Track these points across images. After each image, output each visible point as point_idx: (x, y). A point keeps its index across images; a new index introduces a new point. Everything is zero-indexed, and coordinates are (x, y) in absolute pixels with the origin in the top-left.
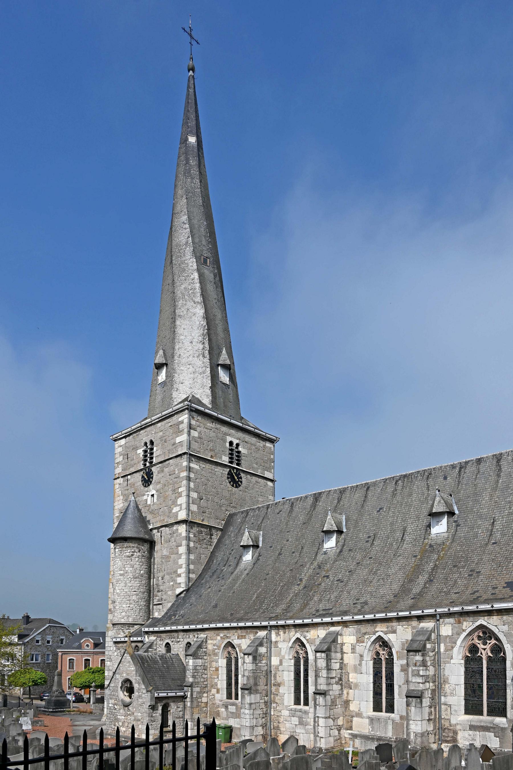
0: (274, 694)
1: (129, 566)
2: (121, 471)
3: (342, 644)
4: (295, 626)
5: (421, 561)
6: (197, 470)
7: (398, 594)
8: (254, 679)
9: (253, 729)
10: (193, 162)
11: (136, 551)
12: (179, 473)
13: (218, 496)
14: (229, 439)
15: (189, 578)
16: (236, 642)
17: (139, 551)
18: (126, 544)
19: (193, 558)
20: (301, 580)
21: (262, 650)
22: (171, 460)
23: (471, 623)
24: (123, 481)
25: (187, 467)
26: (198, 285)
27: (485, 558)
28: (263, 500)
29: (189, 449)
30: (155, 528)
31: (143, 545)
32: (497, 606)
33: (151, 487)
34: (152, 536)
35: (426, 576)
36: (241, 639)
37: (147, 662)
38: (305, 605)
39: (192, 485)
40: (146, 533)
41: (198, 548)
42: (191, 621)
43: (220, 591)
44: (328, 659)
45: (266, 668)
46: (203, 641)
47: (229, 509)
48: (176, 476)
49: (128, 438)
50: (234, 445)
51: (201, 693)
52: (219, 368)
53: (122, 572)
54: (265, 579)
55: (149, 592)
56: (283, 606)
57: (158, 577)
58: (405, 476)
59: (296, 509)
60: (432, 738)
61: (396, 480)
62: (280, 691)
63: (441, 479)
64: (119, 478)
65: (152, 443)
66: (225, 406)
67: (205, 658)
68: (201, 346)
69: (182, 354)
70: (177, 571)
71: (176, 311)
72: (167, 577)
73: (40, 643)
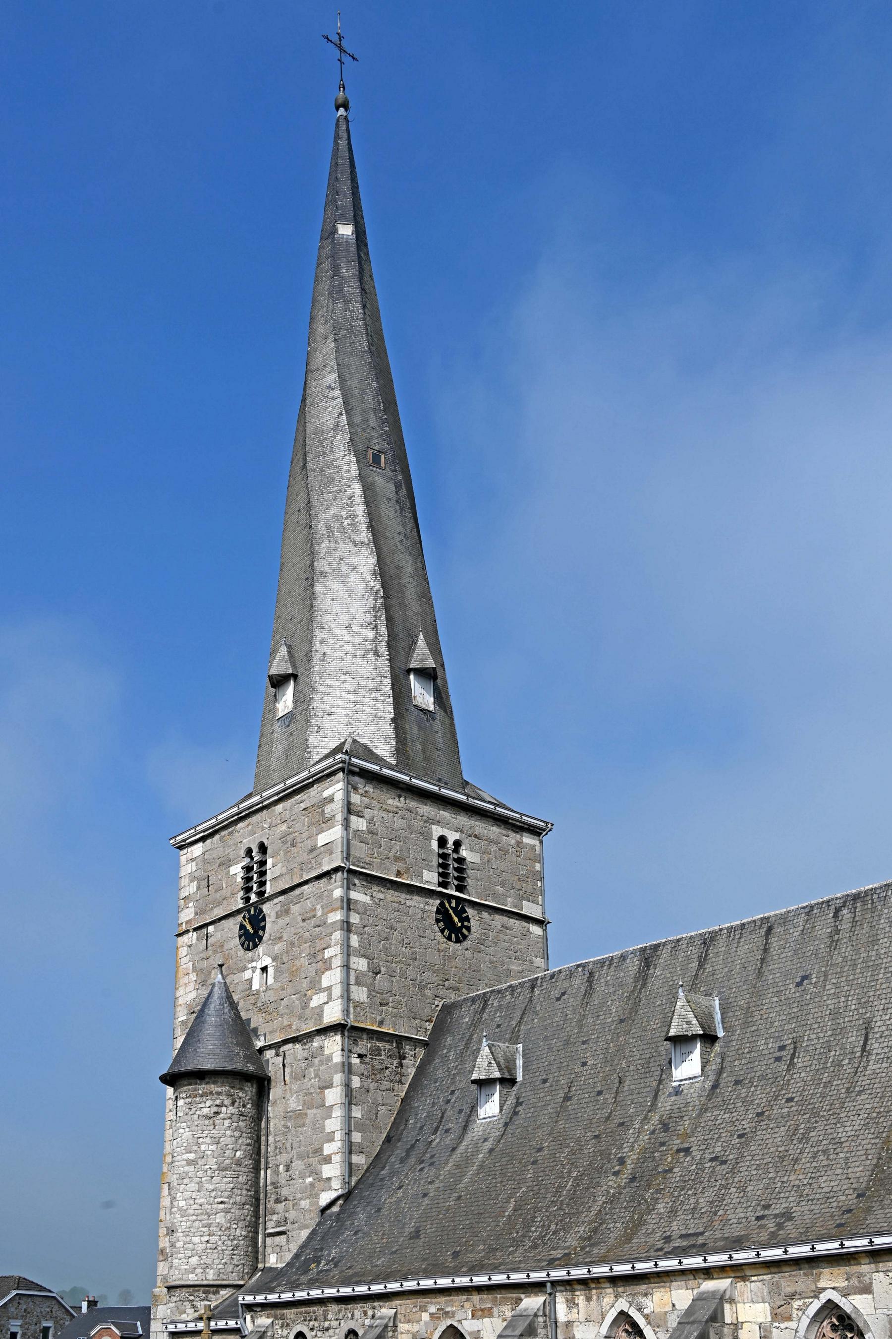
1: (208, 1140)
2: (192, 916)
4: (614, 1280)
7: (868, 1188)
10: (348, 271)
11: (226, 1102)
12: (325, 914)
13: (416, 963)
14: (437, 831)
15: (350, 1164)
17: (233, 1104)
18: (202, 1088)
19: (360, 1116)
20: (622, 1161)
22: (306, 887)
24: (198, 939)
25: (342, 901)
26: (361, 509)
28: (520, 969)
29: (348, 859)
30: (270, 1047)
31: (241, 1089)
33: (261, 949)
34: (262, 1065)
36: (482, 1317)
38: (638, 1225)
39: (355, 940)
40: (248, 1058)
41: (372, 1091)
42: (356, 1274)
43: (425, 1195)
46: (386, 1326)
47: (441, 993)
48: (318, 923)
49: (208, 841)
50: (450, 844)
52: (412, 677)
53: (192, 1156)
54: (535, 1162)
55: (256, 1203)
57: (277, 1166)
58: (856, 897)
59: (600, 988)
64: (187, 932)
65: (263, 848)
66: (427, 759)
68: (371, 634)
71: (316, 564)
72: (298, 1165)
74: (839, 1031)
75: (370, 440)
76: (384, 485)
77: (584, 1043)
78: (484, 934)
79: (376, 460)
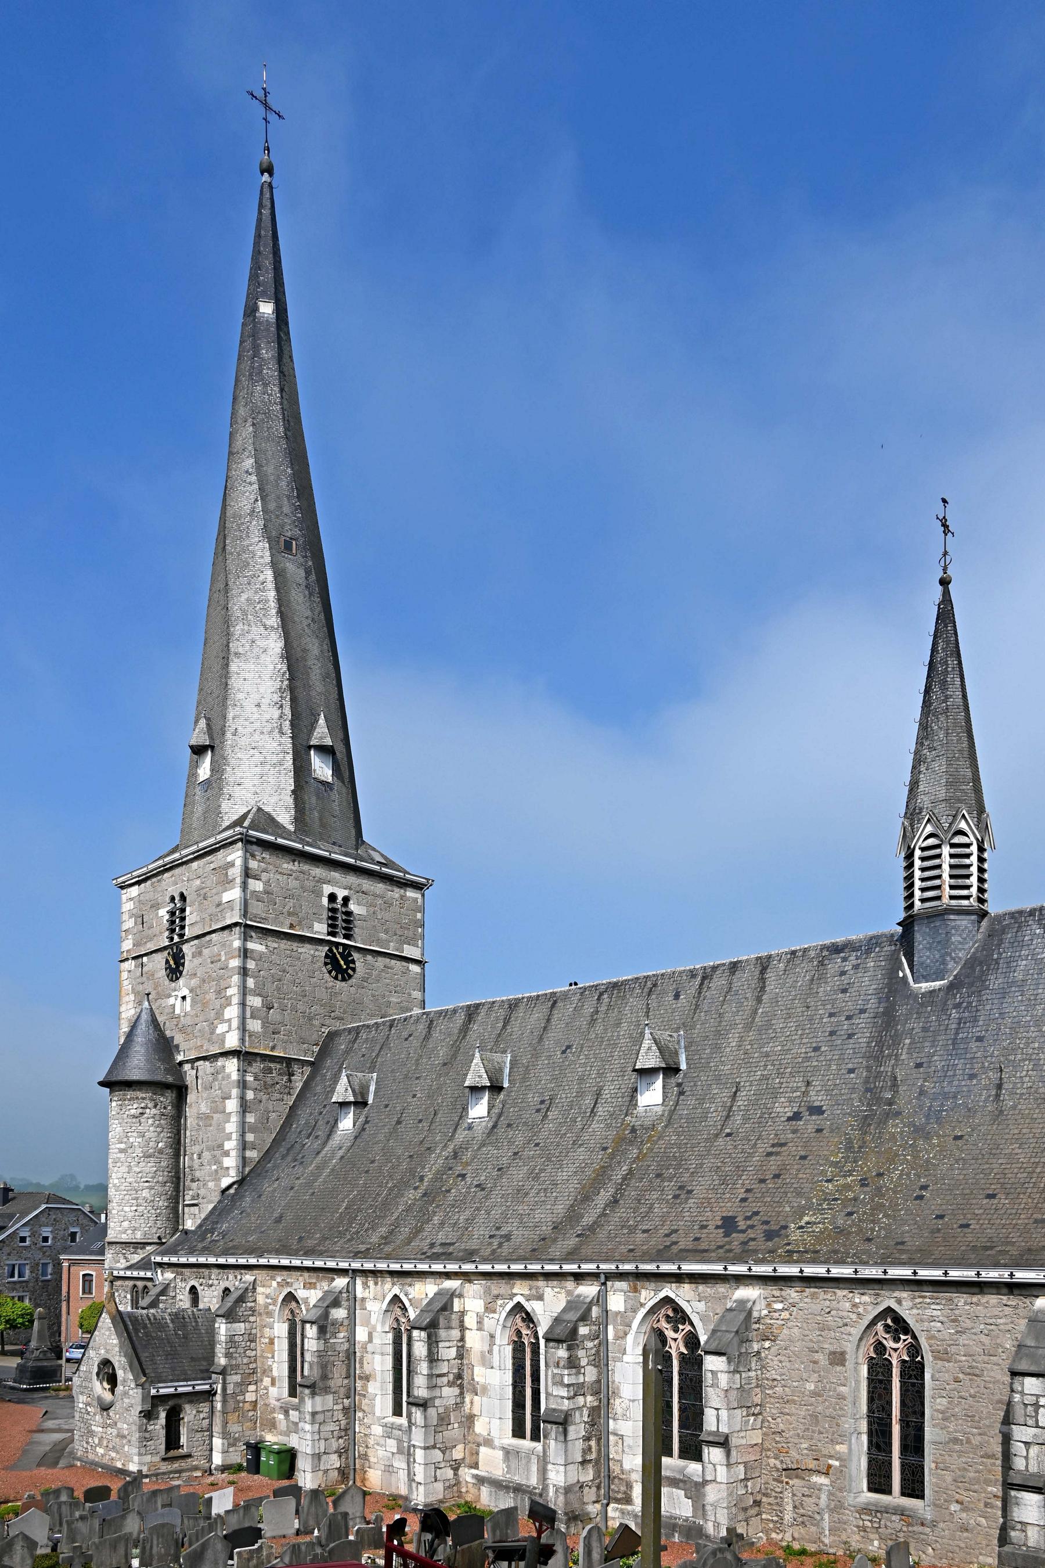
0: (359, 1395)
1: (135, 1134)
2: (131, 946)
3: (463, 1313)
4: (392, 1274)
5: (612, 1159)
6: (261, 954)
7: (561, 1223)
8: (322, 1368)
9: (319, 1459)
10: (267, 353)
11: (149, 1105)
12: (227, 960)
13: (306, 999)
14: (328, 889)
15: (244, 1158)
16: (301, 1294)
17: (155, 1107)
18: (130, 1094)
20: (422, 1179)
21: (339, 1314)
23: (653, 1293)
25: (240, 950)
26: (272, 594)
27: (708, 1163)
28: (399, 1000)
30: (187, 1061)
31: (162, 1095)
32: (688, 1267)
33: (181, 981)
34: (181, 1076)
35: (612, 1191)
36: (309, 1289)
37: (145, 1327)
38: (417, 1231)
39: (251, 983)
40: (168, 1071)
41: (264, 1101)
43: (292, 1188)
44: (432, 1342)
45: (346, 1346)
46: (247, 1289)
47: (327, 1022)
49: (143, 885)
50: (340, 900)
51: (243, 1385)
52: (312, 752)
53: (123, 1146)
54: (367, 1172)
55: (176, 1181)
56: (383, 1230)
58: (615, 985)
59: (436, 1034)
60: (590, 1494)
61: (601, 992)
62: (370, 1390)
63: (670, 997)
64: (127, 959)
65: (183, 898)
66: (323, 825)
67: (252, 1319)
69: (240, 729)
70: (223, 1145)
71: (231, 645)
72: (206, 1155)
73: (28, 1243)
74: (581, 1094)
75: (282, 526)
76: (295, 570)
77: (417, 1078)
78: (368, 974)
79: (288, 546)
